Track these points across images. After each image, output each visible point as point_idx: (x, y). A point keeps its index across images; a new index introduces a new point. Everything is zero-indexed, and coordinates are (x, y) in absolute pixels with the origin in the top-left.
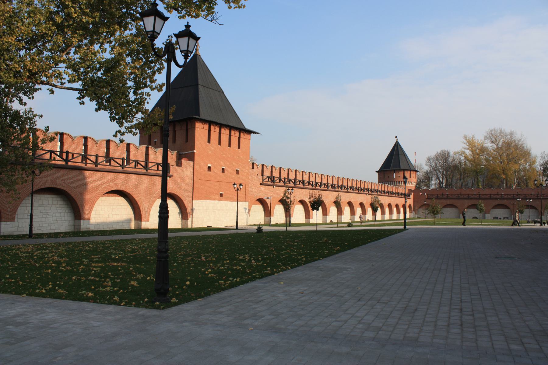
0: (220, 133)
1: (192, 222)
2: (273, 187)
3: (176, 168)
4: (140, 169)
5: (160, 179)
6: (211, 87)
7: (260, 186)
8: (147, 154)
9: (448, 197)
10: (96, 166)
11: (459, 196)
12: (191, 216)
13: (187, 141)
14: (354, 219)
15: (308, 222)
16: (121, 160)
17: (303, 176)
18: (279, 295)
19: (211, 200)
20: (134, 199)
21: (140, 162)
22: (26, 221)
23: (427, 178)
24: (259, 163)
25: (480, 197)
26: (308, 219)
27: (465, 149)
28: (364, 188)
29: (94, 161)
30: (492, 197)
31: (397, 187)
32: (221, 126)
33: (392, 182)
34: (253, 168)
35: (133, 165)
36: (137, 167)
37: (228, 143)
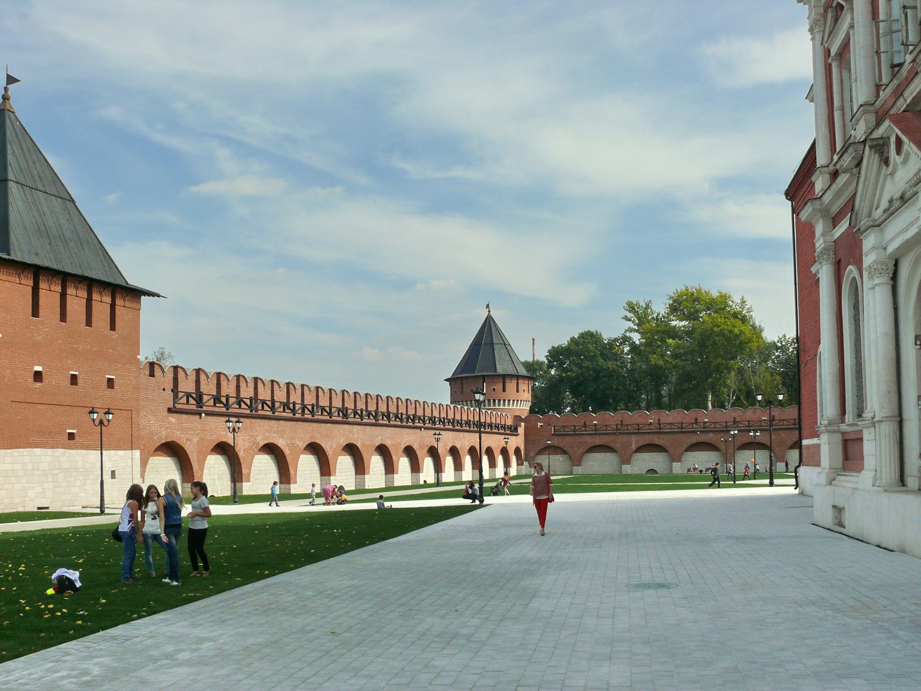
6: (40, 187)
7: (166, 414)
9: (596, 430)
11: (619, 427)
14: (393, 483)
15: (286, 492)
17: (272, 391)
19: (44, 448)
21: (307, 406)
25: (660, 429)
28: (485, 423)
31: (489, 412)
34: (152, 375)
37: (83, 317)
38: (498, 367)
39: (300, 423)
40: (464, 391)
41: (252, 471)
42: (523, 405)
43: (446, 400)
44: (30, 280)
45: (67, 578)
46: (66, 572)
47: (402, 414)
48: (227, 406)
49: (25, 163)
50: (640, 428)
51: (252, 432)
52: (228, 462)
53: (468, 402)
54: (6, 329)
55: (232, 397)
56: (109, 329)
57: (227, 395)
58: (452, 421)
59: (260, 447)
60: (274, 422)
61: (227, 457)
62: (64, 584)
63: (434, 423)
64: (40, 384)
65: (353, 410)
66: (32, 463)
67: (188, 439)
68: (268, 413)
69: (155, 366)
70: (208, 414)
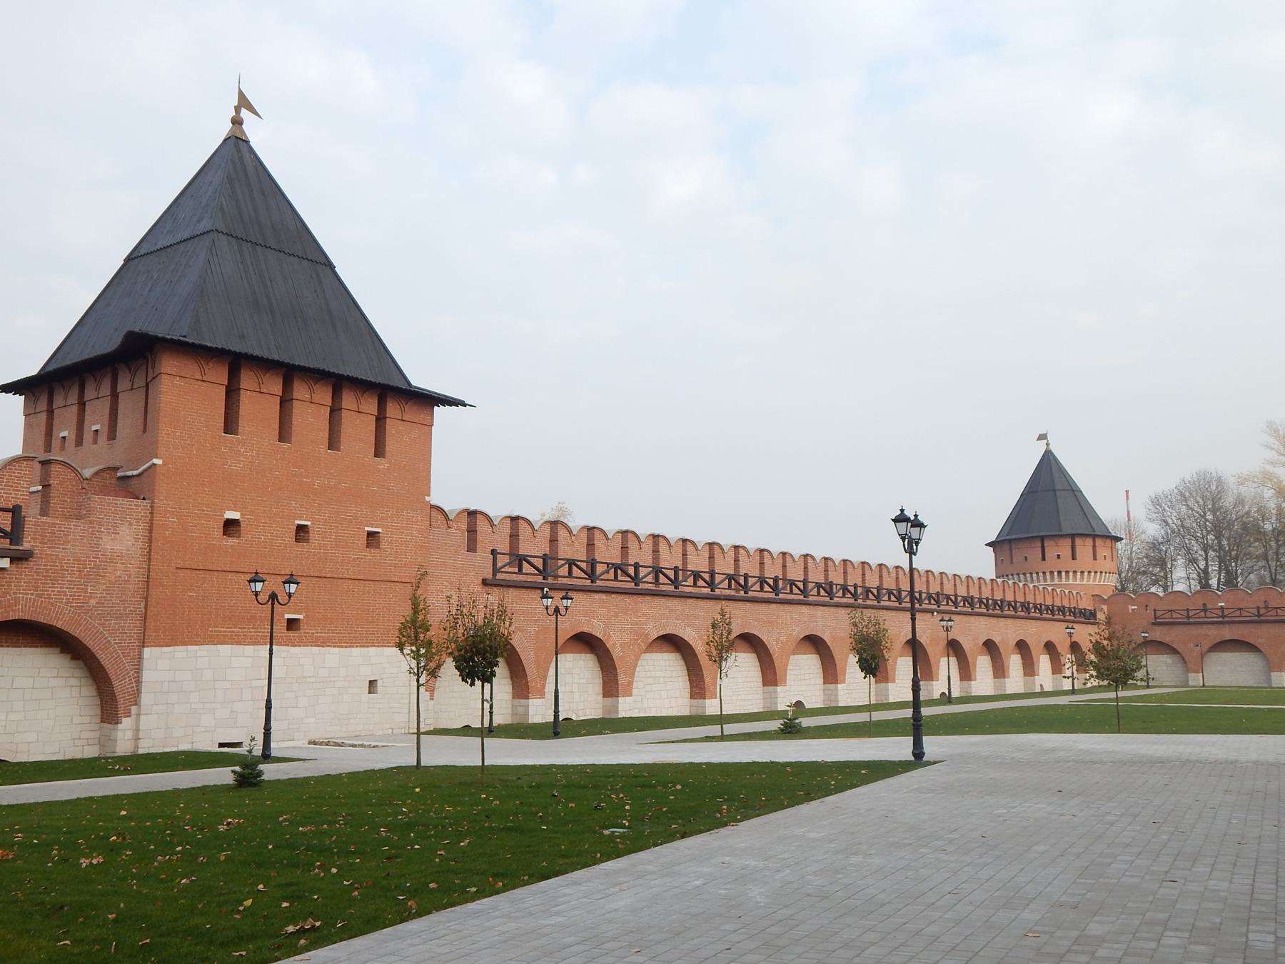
2: (933, 615)
11: (1262, 611)
13: (145, 431)
16: (10, 515)
17: (863, 575)
19: (239, 643)
23: (1158, 560)
27: (1274, 463)
30: (1262, 615)
32: (290, 373)
33: (1037, 573)
38: (1063, 523)
40: (1014, 561)
42: (1104, 580)
43: (988, 571)
47: (920, 593)
50: (1190, 615)
51: (637, 616)
53: (1021, 576)
55: (752, 577)
56: (373, 455)
58: (999, 602)
63: (1028, 610)
64: (235, 540)
66: (300, 665)
68: (530, 579)
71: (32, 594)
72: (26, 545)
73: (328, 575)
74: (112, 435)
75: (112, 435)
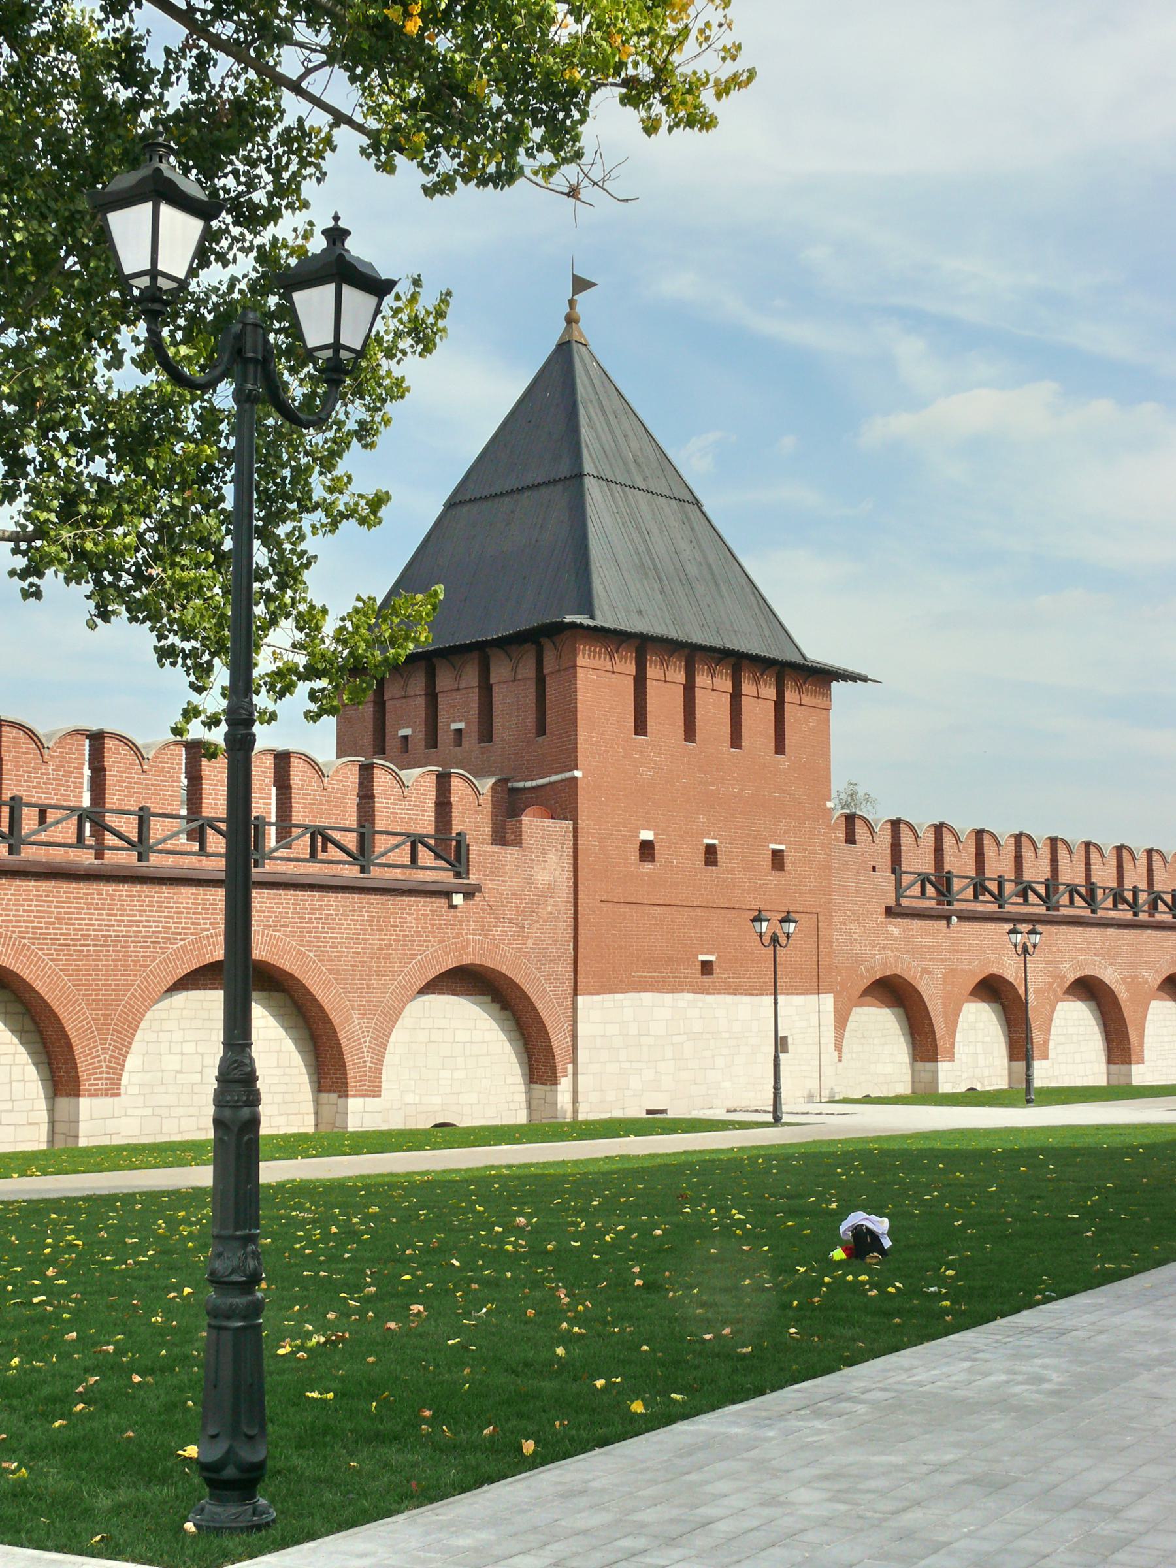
0: (689, 689)
1: (575, 1092)
3: (492, 854)
4: (332, 862)
5: (217, 897)
7: (882, 919)
8: (366, 796)
10: (140, 859)
12: (570, 1067)
15: (1123, 1081)
17: (1088, 864)
18: (804, 1495)
19: (659, 991)
20: (314, 1000)
22: (195, 1091)
24: (880, 814)
26: (1123, 1067)
29: (134, 836)
34: (850, 839)
35: (302, 846)
36: (321, 856)
37: (727, 730)
39: (1149, 932)
41: (1051, 1037)
44: (631, 663)
45: (869, 1231)
46: (867, 1219)
47: (1135, 891)
48: (999, 898)
49: (610, 437)
51: (1051, 953)
52: (1003, 1017)
54: (590, 762)
57: (141, 809)
59: (1067, 985)
60: (1094, 931)
61: (1001, 1007)
62: (864, 1241)
65: (973, 879)
67: (925, 971)
68: (429, 876)
69: (857, 821)
70: (964, 917)
71: (480, 935)
72: (473, 879)
73: (737, 906)
74: (486, 734)
75: (486, 734)
